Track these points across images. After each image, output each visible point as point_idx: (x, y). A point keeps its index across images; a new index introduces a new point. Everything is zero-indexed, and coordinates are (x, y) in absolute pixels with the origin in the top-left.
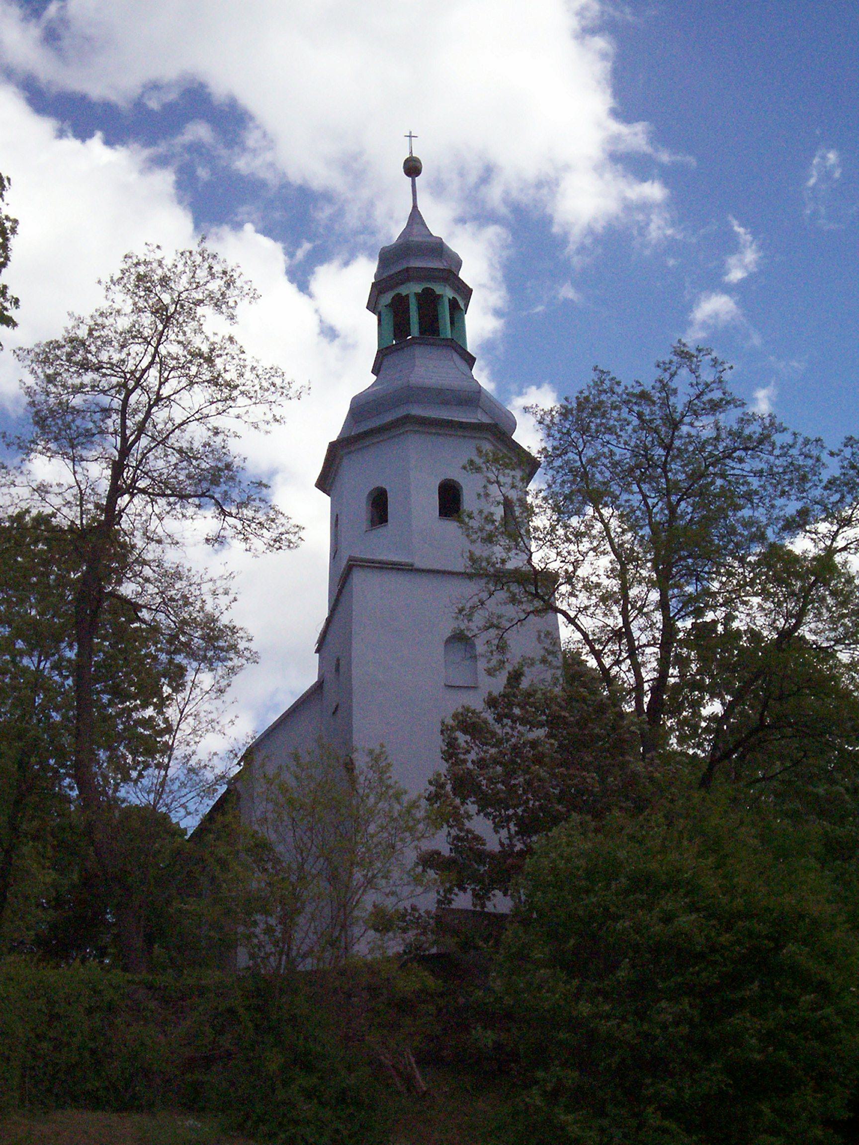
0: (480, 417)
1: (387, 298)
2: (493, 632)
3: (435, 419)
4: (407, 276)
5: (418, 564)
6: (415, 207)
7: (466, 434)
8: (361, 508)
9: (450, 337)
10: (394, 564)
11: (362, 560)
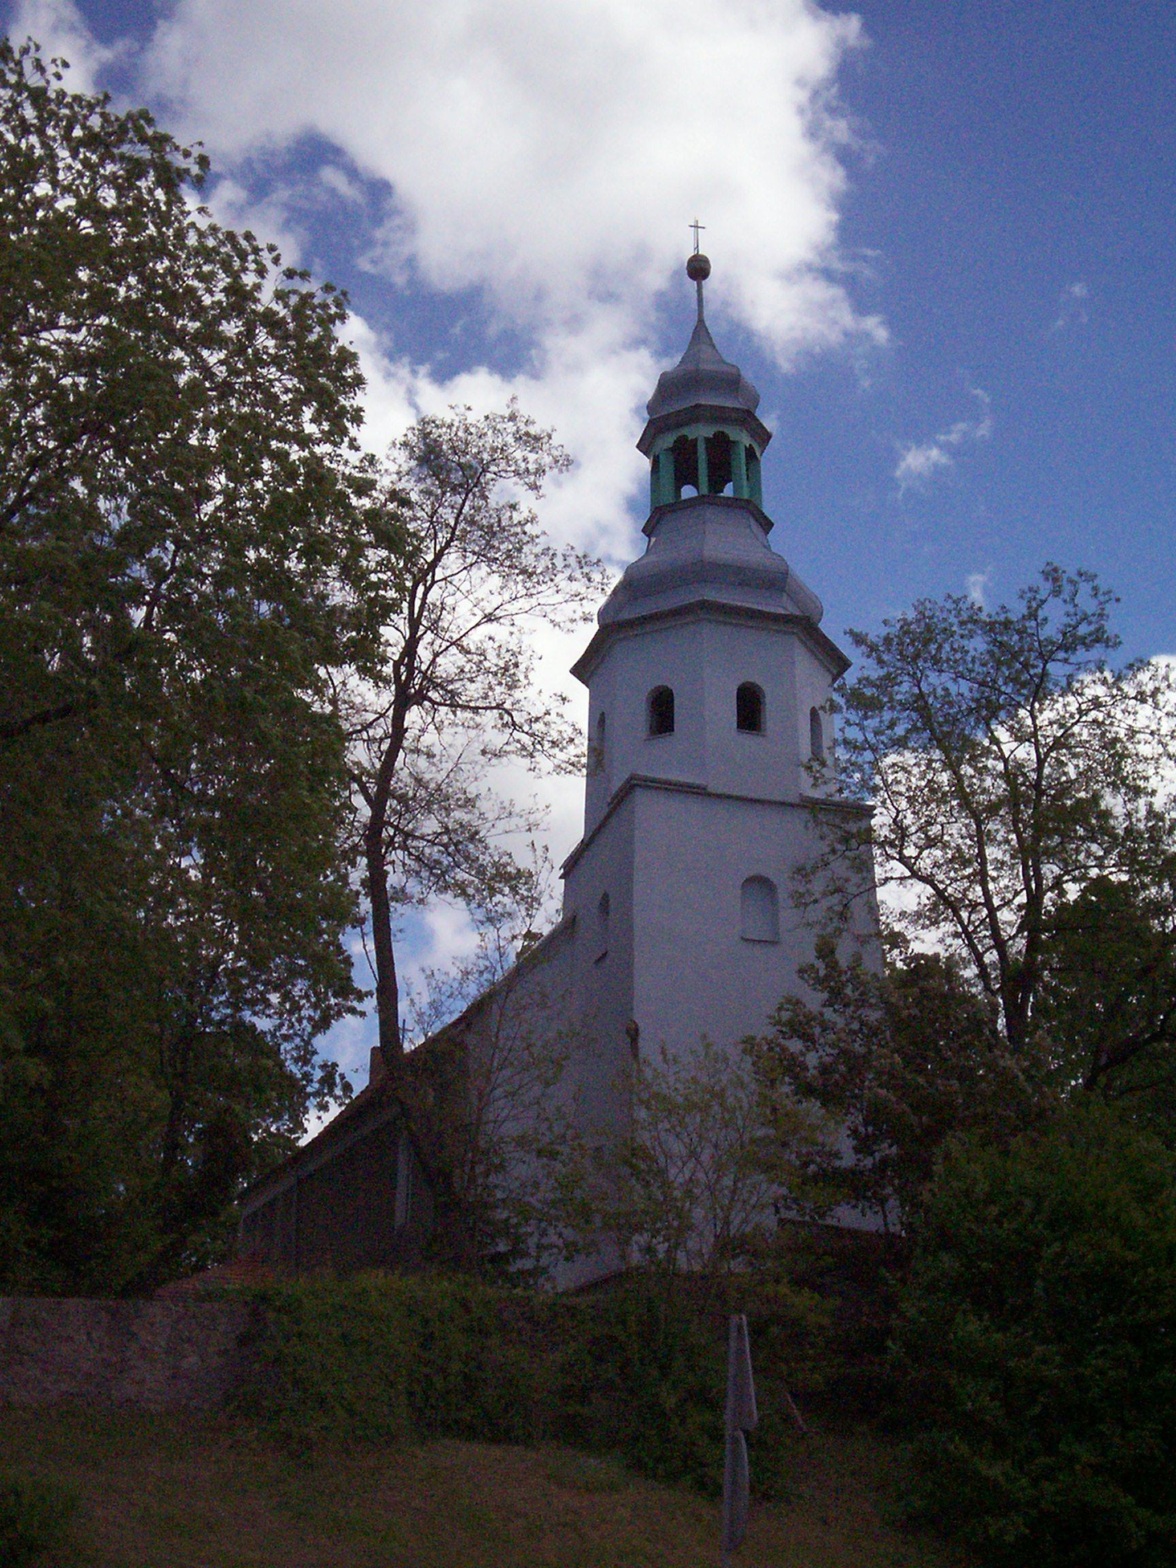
0: (789, 608)
1: (668, 440)
2: (836, 898)
3: (724, 605)
4: (695, 414)
5: (715, 787)
6: (701, 321)
7: (729, 620)
8: (636, 712)
9: (746, 497)
10: (689, 786)
11: (646, 779)
